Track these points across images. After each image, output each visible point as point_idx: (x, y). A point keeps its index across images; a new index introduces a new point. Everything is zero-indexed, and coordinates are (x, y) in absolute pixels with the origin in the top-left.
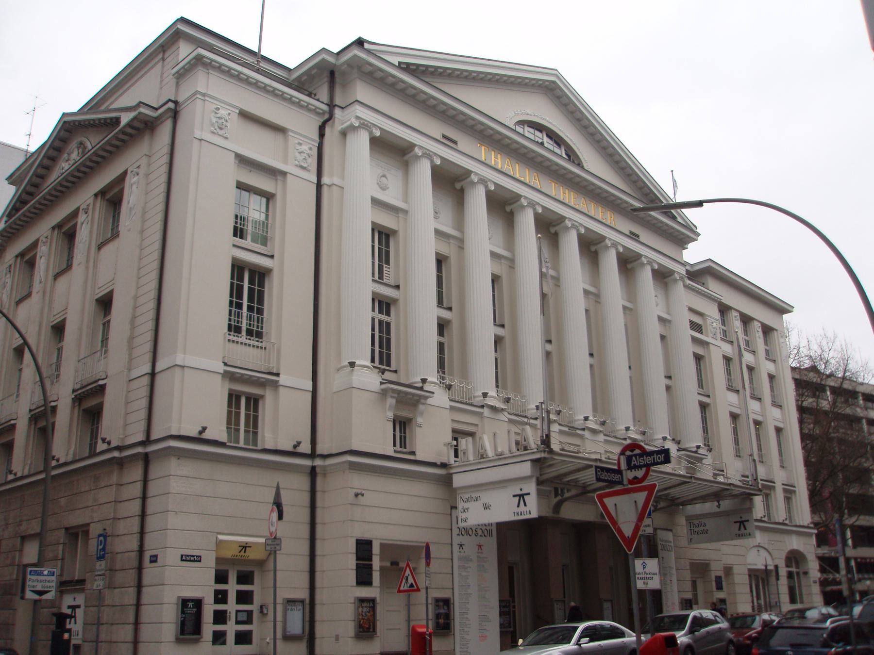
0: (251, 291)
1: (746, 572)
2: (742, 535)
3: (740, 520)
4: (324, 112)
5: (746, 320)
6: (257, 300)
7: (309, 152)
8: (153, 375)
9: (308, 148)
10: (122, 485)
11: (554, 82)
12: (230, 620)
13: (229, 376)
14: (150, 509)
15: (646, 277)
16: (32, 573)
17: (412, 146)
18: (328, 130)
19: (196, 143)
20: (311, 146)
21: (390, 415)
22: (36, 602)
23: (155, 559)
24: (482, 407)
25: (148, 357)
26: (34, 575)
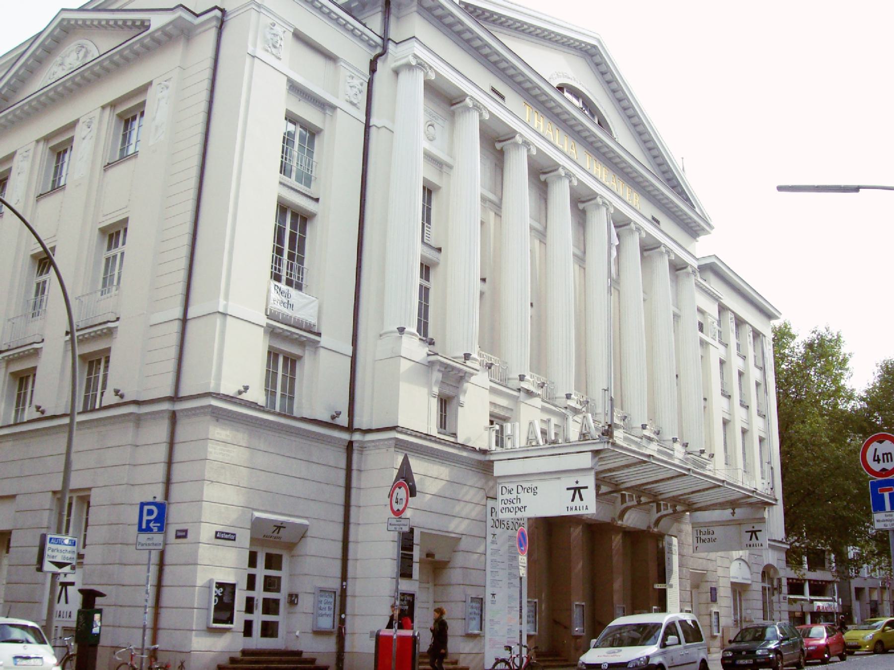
0: (293, 237)
1: (729, 585)
2: (753, 546)
3: (752, 529)
4: (376, 45)
5: (740, 322)
6: (298, 244)
7: (360, 87)
8: (184, 320)
9: (360, 83)
10: (137, 446)
11: (594, 47)
12: (256, 609)
13: (272, 332)
14: (175, 477)
15: (662, 267)
16: (52, 541)
17: (463, 96)
18: (380, 64)
19: (248, 60)
20: (362, 81)
21: (436, 390)
22: (55, 575)
23: (184, 534)
24: (519, 390)
25: (179, 300)
26: (55, 544)
